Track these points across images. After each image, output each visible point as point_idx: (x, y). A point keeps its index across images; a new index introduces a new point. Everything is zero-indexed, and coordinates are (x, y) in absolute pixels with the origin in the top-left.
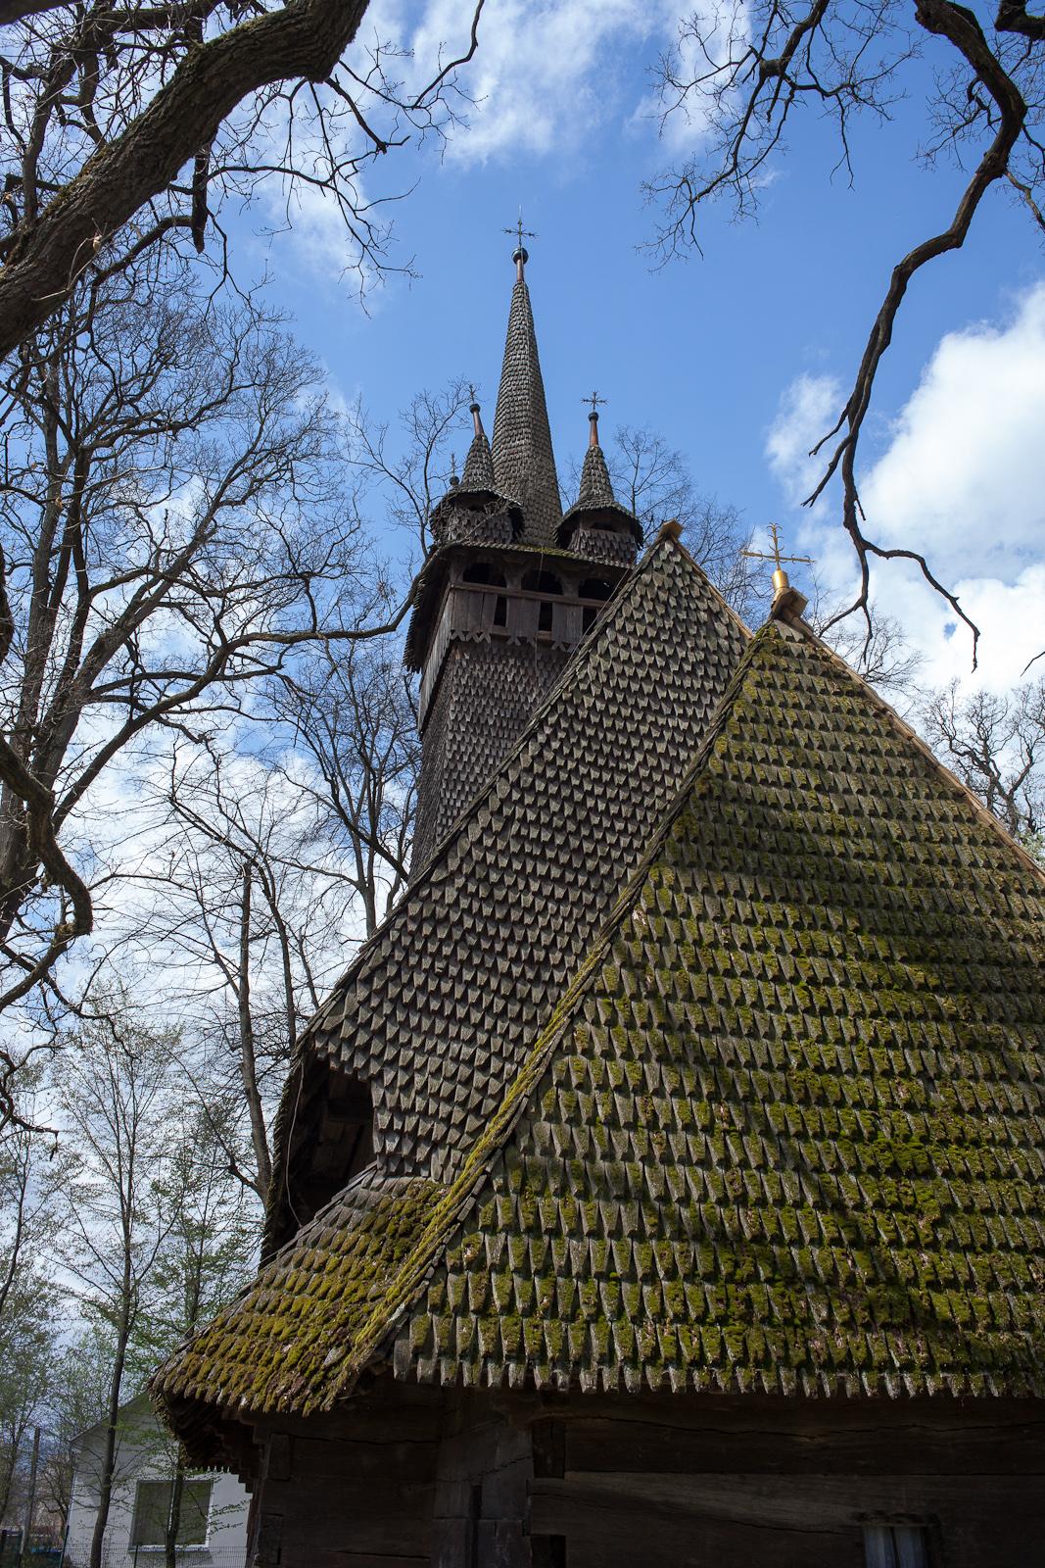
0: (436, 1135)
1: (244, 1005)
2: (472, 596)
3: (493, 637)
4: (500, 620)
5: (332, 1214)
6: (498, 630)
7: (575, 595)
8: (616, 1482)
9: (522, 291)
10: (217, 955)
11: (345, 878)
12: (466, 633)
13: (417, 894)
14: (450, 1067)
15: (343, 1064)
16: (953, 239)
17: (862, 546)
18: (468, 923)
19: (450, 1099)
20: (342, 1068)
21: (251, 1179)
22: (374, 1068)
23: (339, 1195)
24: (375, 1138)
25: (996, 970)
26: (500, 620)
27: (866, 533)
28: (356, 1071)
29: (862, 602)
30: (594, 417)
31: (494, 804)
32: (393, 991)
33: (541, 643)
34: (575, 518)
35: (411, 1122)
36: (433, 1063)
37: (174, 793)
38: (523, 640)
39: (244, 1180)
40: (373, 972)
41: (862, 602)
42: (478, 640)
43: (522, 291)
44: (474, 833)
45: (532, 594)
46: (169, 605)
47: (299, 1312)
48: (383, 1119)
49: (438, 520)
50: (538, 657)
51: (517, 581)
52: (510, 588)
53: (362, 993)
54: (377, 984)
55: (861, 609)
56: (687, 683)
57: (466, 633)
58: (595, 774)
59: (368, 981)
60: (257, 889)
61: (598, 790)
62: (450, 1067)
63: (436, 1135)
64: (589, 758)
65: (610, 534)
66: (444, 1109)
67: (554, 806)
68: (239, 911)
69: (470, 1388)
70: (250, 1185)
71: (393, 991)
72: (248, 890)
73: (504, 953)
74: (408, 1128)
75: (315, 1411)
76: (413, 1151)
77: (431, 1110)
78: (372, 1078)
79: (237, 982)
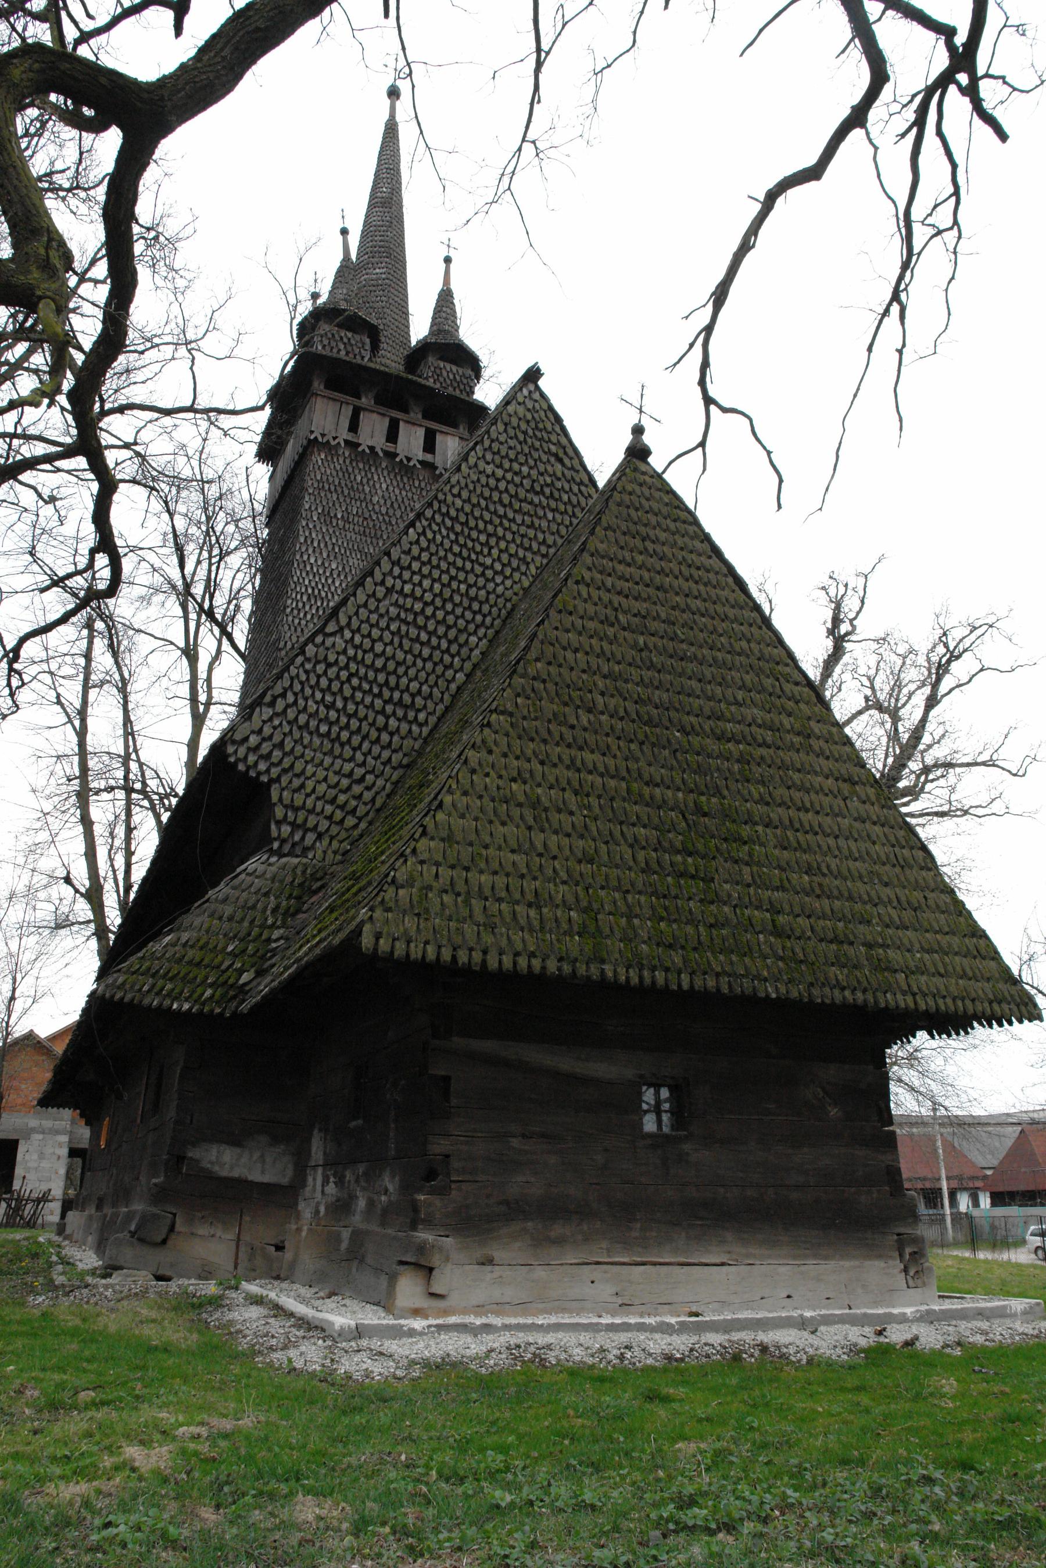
0: (322, 828)
1: (82, 744)
2: (331, 403)
3: (346, 442)
4: (354, 427)
5: (236, 882)
6: (350, 437)
7: (420, 416)
8: (488, 1046)
9: (391, 131)
10: (58, 696)
11: (172, 643)
12: (323, 435)
13: (313, 641)
14: (333, 779)
15: (248, 768)
16: (813, 173)
17: (708, 401)
18: (353, 667)
19: (333, 801)
20: (248, 768)
21: (83, 890)
22: (275, 772)
23: (243, 867)
24: (273, 827)
25: (770, 733)
26: (354, 427)
27: (712, 393)
28: (259, 774)
29: (702, 444)
30: (448, 260)
31: (378, 576)
32: (291, 714)
33: (387, 454)
34: (425, 347)
35: (301, 815)
36: (321, 774)
37: (34, 547)
38: (372, 448)
39: (77, 891)
40: (275, 698)
41: (702, 444)
42: (333, 443)
43: (391, 131)
44: (361, 597)
45: (382, 410)
46: (27, 370)
47: (216, 947)
48: (279, 812)
49: (306, 329)
50: (384, 465)
51: (371, 395)
52: (364, 401)
53: (267, 712)
54: (280, 705)
55: (700, 449)
56: (536, 500)
57: (323, 435)
58: (459, 563)
59: (272, 704)
60: (100, 645)
61: (461, 576)
62: (333, 779)
63: (322, 828)
64: (456, 549)
65: (454, 368)
66: (329, 809)
67: (426, 583)
68: (82, 661)
69: (416, 961)
70: (82, 895)
71: (291, 714)
72: (90, 643)
73: (380, 695)
74: (299, 821)
75: (234, 1014)
76: (303, 838)
77: (318, 809)
78: (271, 781)
79: (77, 723)
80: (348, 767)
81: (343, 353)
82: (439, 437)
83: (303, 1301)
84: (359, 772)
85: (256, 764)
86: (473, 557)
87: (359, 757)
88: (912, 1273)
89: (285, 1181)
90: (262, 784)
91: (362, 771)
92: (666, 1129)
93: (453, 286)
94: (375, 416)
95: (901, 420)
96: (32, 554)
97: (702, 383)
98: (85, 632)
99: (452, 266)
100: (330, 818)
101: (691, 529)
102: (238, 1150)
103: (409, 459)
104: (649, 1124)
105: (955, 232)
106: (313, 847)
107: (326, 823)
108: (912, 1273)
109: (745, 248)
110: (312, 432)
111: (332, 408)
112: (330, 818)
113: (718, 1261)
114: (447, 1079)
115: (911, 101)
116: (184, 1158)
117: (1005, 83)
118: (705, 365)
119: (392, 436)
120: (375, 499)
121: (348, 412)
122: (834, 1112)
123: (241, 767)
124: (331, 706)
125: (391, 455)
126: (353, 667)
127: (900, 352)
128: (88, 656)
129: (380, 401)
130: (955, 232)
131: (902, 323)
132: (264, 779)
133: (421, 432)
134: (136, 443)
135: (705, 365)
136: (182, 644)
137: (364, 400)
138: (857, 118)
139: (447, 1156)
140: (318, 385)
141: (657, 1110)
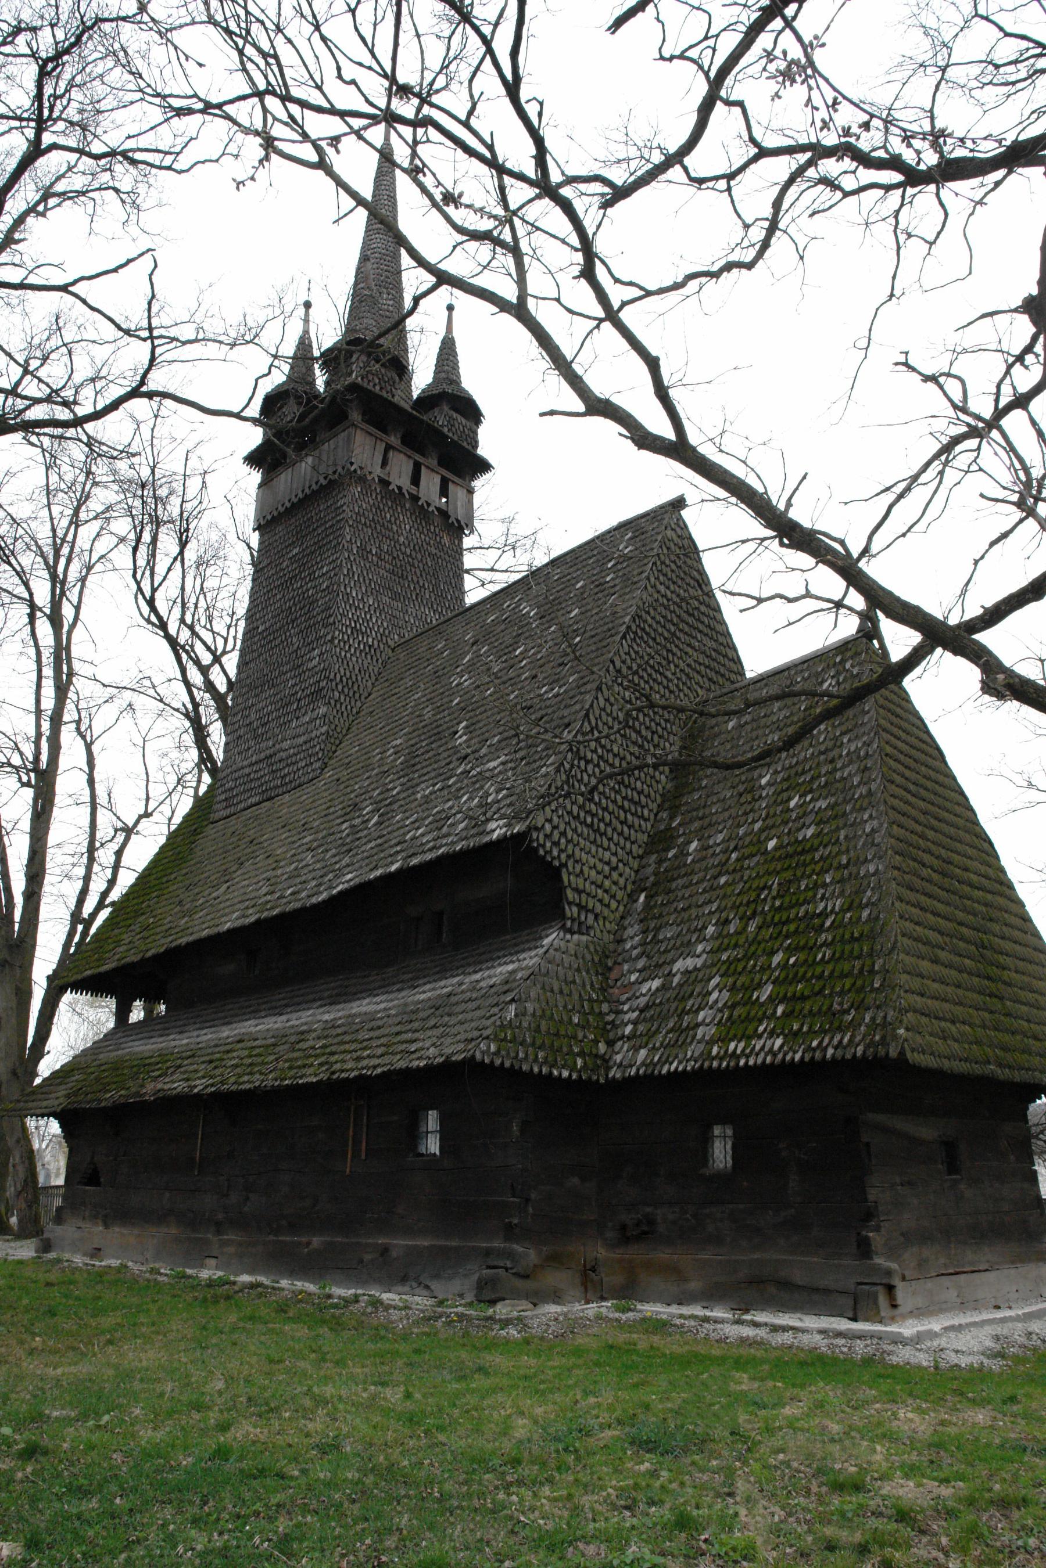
7: (435, 462)
15: (546, 852)
28: (553, 858)
38: (400, 488)
57: (361, 468)
81: (378, 388)
82: (451, 486)
83: (658, 1313)
93: (456, 334)
94: (402, 456)
95: (115, 270)
99: (454, 313)
101: (903, 703)
103: (429, 505)
105: (975, 454)
110: (352, 464)
111: (369, 441)
119: (416, 480)
120: (402, 539)
121: (381, 447)
123: (541, 852)
125: (415, 498)
127: (976, 562)
130: (975, 454)
131: (993, 544)
132: (556, 863)
133: (437, 479)
134: (75, 403)
140: (355, 416)
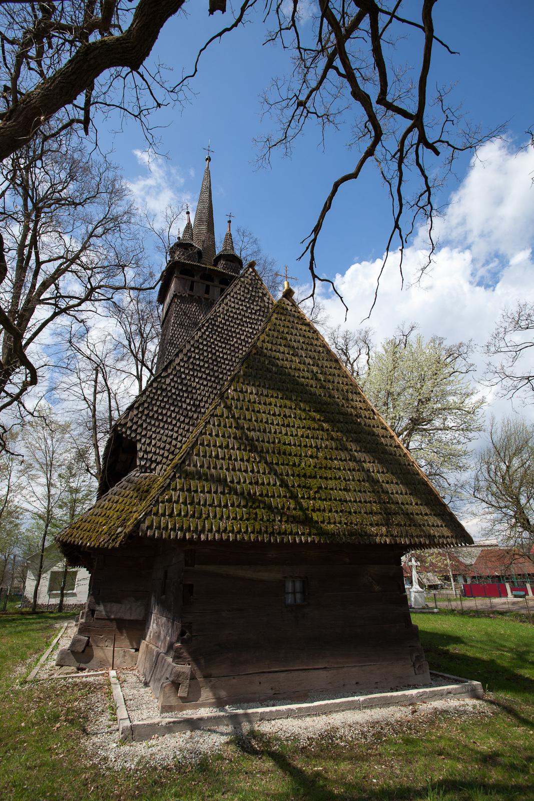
10: (85, 398)
16: (354, 176)
18: (173, 391)
28: (132, 438)
32: (146, 412)
35: (150, 456)
45: (203, 281)
48: (140, 454)
52: (196, 278)
53: (135, 412)
58: (220, 344)
59: (138, 408)
61: (221, 350)
67: (205, 354)
68: (93, 383)
70: (94, 475)
75: (113, 547)
76: (150, 465)
79: (92, 407)
80: (170, 433)
84: (175, 435)
85: (130, 434)
86: (226, 341)
87: (176, 429)
88: (417, 667)
89: (141, 618)
90: (133, 442)
91: (176, 435)
92: (298, 601)
96: (70, 342)
97: (311, 268)
98: (94, 372)
100: (162, 455)
102: (120, 605)
104: (290, 599)
106: (155, 468)
107: (161, 458)
108: (417, 667)
109: (327, 207)
112: (162, 455)
113: (322, 667)
114: (191, 586)
115: (407, 152)
116: (95, 611)
117: (449, 145)
118: (313, 259)
122: (377, 588)
124: (164, 408)
126: (173, 391)
128: (96, 381)
129: (202, 278)
135: (313, 259)
136: (136, 374)
137: (195, 278)
138: (370, 152)
139: (190, 623)
141: (294, 593)
